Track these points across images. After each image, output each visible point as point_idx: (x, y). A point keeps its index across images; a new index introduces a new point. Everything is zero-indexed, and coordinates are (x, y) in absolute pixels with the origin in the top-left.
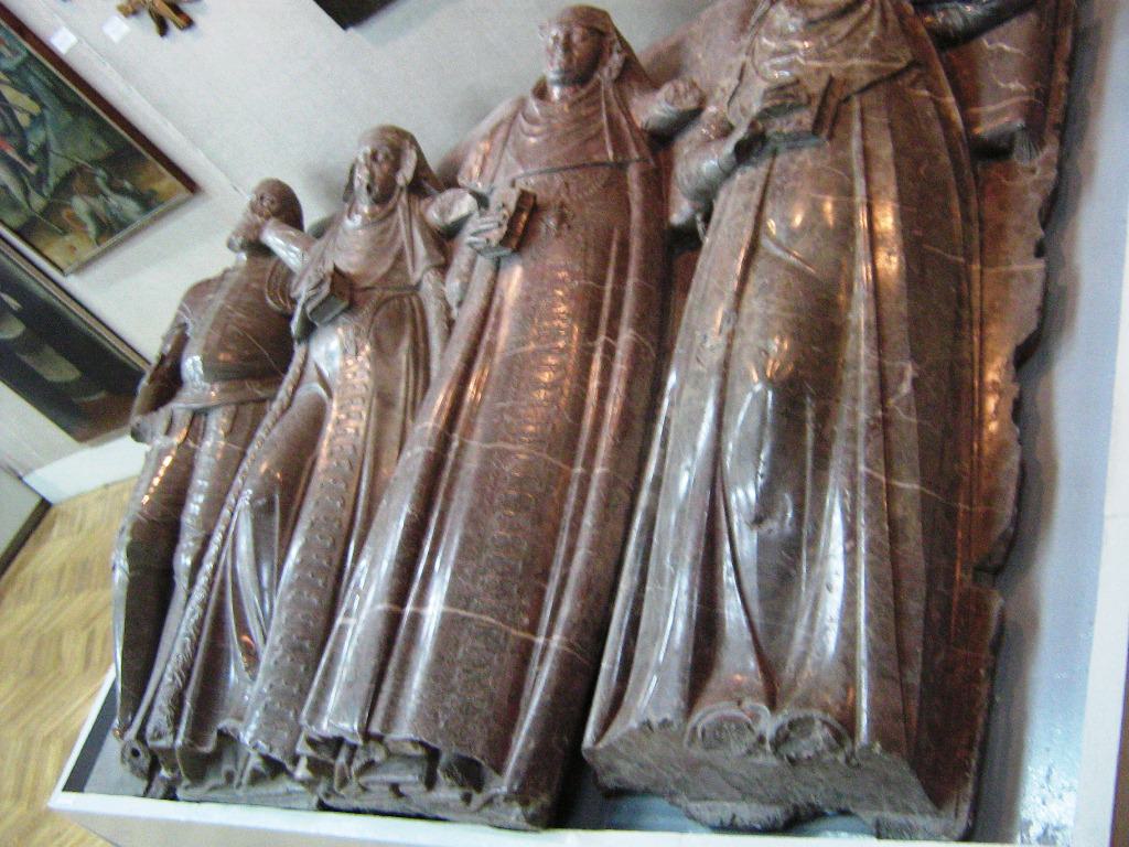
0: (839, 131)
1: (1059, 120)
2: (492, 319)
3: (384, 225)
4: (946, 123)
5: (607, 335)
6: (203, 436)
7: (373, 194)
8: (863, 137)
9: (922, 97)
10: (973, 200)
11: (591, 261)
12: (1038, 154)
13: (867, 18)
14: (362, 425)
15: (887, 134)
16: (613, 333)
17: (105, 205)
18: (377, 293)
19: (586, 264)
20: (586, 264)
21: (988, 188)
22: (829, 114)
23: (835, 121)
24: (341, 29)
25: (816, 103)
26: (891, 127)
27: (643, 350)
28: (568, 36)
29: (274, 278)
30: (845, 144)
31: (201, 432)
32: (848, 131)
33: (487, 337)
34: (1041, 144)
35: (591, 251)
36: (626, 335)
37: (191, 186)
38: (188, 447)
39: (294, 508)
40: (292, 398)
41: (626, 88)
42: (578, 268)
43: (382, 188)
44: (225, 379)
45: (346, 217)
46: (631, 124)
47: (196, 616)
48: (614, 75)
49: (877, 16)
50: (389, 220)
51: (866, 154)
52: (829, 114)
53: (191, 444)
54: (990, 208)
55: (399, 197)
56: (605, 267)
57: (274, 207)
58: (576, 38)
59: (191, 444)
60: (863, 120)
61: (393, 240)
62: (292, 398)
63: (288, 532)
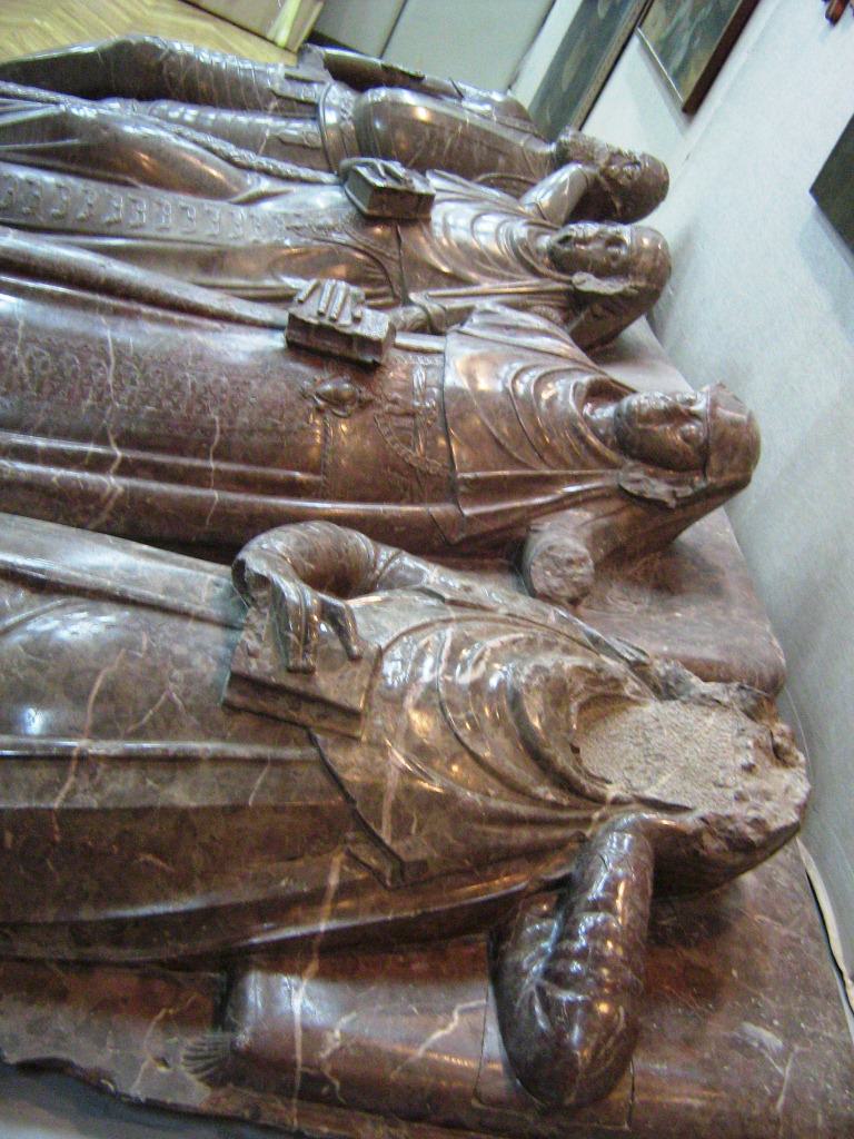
0: (242, 721)
1: (267, 1118)
2: (177, 317)
3: (513, 263)
4: (277, 909)
5: (124, 461)
6: (285, 117)
7: (558, 246)
8: (217, 760)
9: (326, 875)
10: (128, 954)
11: (256, 439)
12: (196, 1072)
13: (519, 791)
14: (173, 234)
15: (220, 800)
16: (126, 469)
17: (684, 30)
18: (392, 252)
19: (251, 432)
20: (251, 432)
21: (159, 987)
22: (280, 707)
23: (266, 718)
24: (810, 186)
25: (292, 682)
26: (236, 810)
27: (92, 507)
28: (693, 416)
29: (514, 183)
30: (208, 730)
31: (287, 114)
32: (239, 738)
33: (146, 310)
34: (213, 1081)
35: (276, 439)
36: (113, 483)
37: (692, 107)
38: (267, 101)
39: (59, 164)
40: (250, 169)
41: (614, 505)
42: (243, 419)
43: (568, 256)
44: (358, 133)
45: (525, 221)
46: (540, 511)
47: (520, 324)
48: (628, 487)
49: (523, 809)
50: (522, 270)
51: (185, 761)
52: (280, 707)
53: (274, 104)
54: (112, 983)
55: (559, 281)
56: (246, 460)
57: (623, 181)
58: (691, 428)
59: (274, 104)
60: (260, 762)
61: (487, 274)
62: (250, 169)
63: (24, 158)
